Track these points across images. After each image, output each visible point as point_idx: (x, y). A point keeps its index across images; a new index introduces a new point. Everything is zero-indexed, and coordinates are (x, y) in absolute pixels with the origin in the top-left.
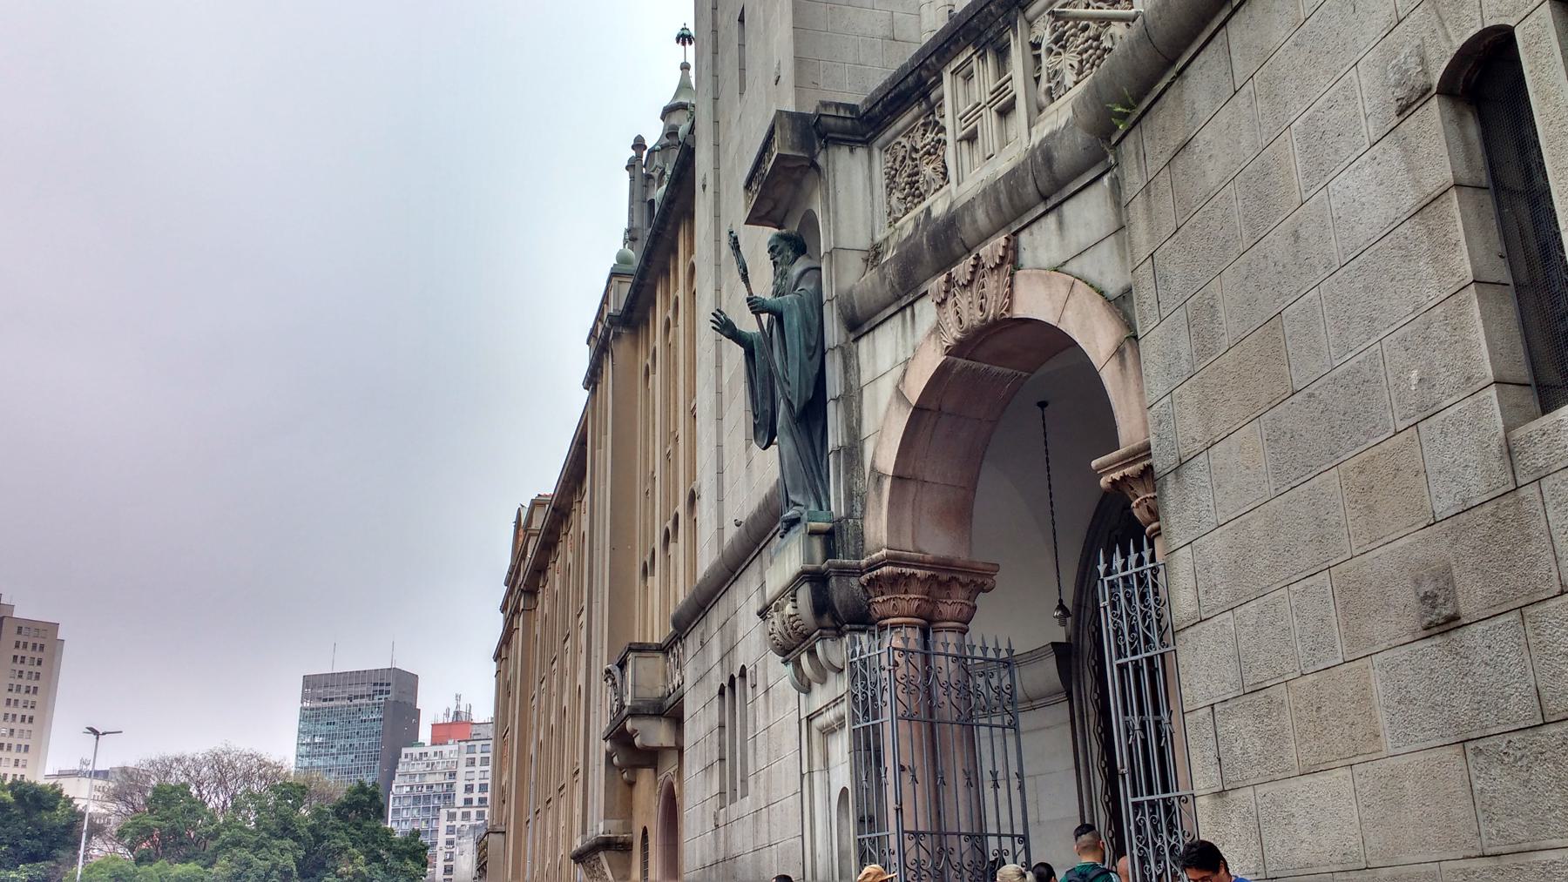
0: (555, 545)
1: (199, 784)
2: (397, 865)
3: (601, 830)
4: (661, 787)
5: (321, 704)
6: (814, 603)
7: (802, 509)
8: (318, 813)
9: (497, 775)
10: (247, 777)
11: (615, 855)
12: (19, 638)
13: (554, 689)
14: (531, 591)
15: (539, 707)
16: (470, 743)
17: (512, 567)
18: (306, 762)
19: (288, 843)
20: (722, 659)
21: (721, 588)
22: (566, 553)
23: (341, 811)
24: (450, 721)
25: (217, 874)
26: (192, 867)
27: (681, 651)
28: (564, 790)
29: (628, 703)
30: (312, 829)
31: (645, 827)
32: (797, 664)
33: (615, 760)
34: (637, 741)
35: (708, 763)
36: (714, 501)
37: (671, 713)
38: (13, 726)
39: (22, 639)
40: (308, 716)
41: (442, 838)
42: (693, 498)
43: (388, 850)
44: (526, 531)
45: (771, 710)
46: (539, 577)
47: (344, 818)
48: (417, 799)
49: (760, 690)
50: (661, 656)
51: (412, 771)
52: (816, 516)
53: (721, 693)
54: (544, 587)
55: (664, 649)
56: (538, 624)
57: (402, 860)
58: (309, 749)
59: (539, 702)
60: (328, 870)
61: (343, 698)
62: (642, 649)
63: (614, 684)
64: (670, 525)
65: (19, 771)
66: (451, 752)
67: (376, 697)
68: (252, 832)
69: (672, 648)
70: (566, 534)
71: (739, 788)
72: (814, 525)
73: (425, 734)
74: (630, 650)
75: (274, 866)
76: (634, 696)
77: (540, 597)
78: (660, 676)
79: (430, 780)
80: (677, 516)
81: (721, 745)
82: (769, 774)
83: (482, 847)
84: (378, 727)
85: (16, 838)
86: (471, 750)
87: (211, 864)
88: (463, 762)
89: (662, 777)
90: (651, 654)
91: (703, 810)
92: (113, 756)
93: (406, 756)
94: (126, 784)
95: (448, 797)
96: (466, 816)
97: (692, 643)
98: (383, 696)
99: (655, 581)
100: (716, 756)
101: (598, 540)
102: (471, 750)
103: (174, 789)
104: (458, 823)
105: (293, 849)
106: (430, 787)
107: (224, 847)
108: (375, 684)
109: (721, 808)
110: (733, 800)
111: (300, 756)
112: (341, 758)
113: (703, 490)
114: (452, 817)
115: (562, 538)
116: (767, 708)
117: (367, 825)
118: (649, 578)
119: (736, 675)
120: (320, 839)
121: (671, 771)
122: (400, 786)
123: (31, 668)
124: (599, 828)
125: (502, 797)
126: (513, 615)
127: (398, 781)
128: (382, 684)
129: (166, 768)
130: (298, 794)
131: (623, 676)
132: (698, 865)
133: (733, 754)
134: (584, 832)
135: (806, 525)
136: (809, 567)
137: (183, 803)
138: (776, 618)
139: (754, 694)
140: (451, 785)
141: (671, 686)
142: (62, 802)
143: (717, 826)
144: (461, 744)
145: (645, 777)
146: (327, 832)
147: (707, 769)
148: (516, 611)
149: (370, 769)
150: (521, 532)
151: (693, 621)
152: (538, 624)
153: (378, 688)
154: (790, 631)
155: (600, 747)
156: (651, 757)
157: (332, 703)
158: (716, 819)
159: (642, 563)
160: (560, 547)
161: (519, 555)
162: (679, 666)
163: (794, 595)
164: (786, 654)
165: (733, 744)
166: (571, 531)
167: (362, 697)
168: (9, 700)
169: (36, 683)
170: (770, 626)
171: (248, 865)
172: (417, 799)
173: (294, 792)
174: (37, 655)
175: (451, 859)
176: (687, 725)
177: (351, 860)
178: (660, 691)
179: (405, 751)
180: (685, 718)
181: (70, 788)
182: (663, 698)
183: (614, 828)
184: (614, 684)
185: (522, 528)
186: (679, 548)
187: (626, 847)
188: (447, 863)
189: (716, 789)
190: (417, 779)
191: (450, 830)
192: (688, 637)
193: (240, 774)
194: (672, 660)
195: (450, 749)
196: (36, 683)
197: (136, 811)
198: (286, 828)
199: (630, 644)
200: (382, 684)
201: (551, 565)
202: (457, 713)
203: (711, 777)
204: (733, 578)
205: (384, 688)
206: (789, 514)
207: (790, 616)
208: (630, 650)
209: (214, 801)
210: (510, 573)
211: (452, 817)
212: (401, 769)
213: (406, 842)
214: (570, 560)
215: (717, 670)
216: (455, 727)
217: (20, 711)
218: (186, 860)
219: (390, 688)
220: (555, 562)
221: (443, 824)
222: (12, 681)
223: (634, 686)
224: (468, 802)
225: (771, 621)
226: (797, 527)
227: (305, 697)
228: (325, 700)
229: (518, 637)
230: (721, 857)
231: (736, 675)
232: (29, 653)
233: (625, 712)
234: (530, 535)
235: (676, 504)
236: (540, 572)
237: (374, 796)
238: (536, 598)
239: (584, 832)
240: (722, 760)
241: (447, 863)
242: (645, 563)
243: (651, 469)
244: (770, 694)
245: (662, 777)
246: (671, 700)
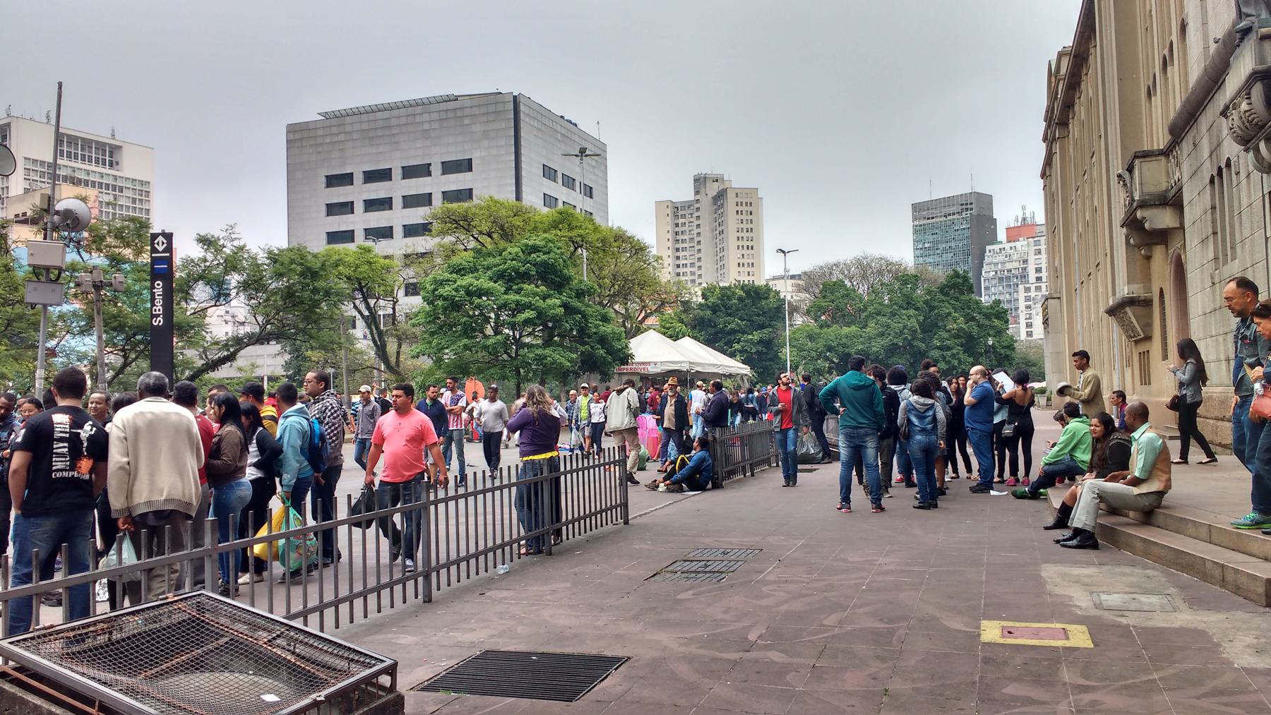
0: (1079, 84)
1: (851, 279)
2: (987, 322)
3: (1126, 292)
4: (1172, 258)
5: (926, 222)
6: (1266, 97)
7: (1253, 19)
8: (929, 292)
9: (1051, 258)
10: (880, 272)
11: (1138, 310)
12: (737, 200)
13: (1087, 194)
14: (1064, 123)
15: (1077, 210)
16: (1036, 239)
17: (1048, 107)
18: (921, 260)
19: (912, 312)
20: (1211, 155)
21: (1206, 98)
22: (1088, 87)
23: (944, 290)
24: (1019, 224)
25: (869, 332)
26: (853, 328)
27: (1179, 152)
28: (1100, 267)
29: (1137, 198)
30: (926, 302)
31: (1161, 289)
32: (1257, 151)
33: (1132, 241)
34: (1147, 226)
35: (1204, 237)
36: (1199, 25)
37: (1174, 201)
38: (743, 252)
39: (739, 200)
40: (917, 231)
41: (1022, 304)
42: (1183, 27)
43: (979, 313)
44: (1056, 77)
45: (1252, 191)
46: (1069, 112)
47: (946, 294)
48: (1001, 279)
49: (1243, 175)
50: (1163, 159)
51: (995, 261)
52: (1267, 22)
53: (1212, 181)
54: (1073, 118)
55: (1166, 153)
56: (1071, 147)
57: (990, 320)
58: (922, 251)
59: (1077, 205)
60: (940, 328)
61: (941, 216)
62: (1146, 155)
63: (1125, 185)
64: (1166, 52)
65: (751, 278)
66: (1022, 246)
67: (964, 213)
68: (887, 306)
69: (1172, 151)
70: (1087, 74)
71: (1229, 253)
72: (1263, 30)
73: (1002, 235)
74: (1136, 157)
75: (905, 327)
76: (1142, 191)
77: (1071, 126)
78: (1163, 174)
79: (1009, 266)
80: (1171, 43)
81: (1214, 222)
82: (1252, 241)
83: (1045, 309)
84: (967, 233)
85: (751, 316)
86: (1037, 243)
87: (865, 326)
88: (1032, 252)
89: (1172, 250)
90: (1154, 158)
91: (1202, 271)
92: (798, 265)
93: (990, 251)
94: (807, 280)
95: (1024, 277)
96: (1038, 289)
97: (1186, 146)
98: (969, 212)
99: (1157, 100)
100: (1210, 231)
101: (1108, 73)
102: (1037, 243)
103: (835, 283)
104: (1033, 294)
105: (916, 316)
106: (1010, 271)
107: (870, 316)
108: (962, 205)
109: (1216, 270)
110: (1225, 263)
111: (916, 257)
112: (944, 255)
113: (1190, 18)
114: (1028, 290)
115: (1084, 78)
116: (1249, 191)
117: (963, 297)
118: (1153, 98)
119: (1223, 166)
120: (932, 308)
121: (1179, 245)
122: (988, 272)
123: (747, 217)
124: (1124, 291)
125: (1055, 273)
126: (1052, 143)
127: (985, 268)
128: (967, 204)
129: (831, 268)
130: (913, 280)
131: (1132, 178)
132: (1200, 313)
133: (1223, 228)
134: (1114, 294)
135: (1257, 32)
136: (1260, 67)
137: (842, 292)
138: (1235, 115)
139: (1238, 179)
140: (1025, 269)
141: (1173, 181)
142: (772, 294)
143: (1213, 283)
144: (1030, 240)
145: (1158, 252)
146: (936, 304)
147: (1204, 241)
148: (1054, 139)
149: (965, 262)
150: (1053, 79)
151: (1186, 127)
152: (1071, 147)
153: (964, 207)
154: (1247, 124)
155: (1120, 234)
156: (1162, 237)
157: (933, 220)
158: (1212, 278)
159: (1146, 87)
160: (1083, 86)
161: (1052, 96)
162: (1178, 164)
163: (1249, 94)
164: (1248, 143)
165: (1223, 220)
166: (1090, 72)
167: (954, 214)
168: (738, 237)
169: (751, 226)
170: (1230, 122)
171: (888, 326)
172: (1001, 279)
173: (906, 279)
174: (749, 209)
175: (1030, 318)
176: (1186, 210)
177: (955, 320)
178: (1164, 186)
179: (988, 248)
180: (1185, 205)
181: (779, 286)
182: (1167, 191)
183: (1137, 290)
184: (1125, 185)
185: (1053, 75)
186: (1173, 71)
187: (1147, 303)
188: (1028, 321)
189: (1211, 255)
190: (1000, 266)
191: (1028, 299)
192: (1183, 142)
193: (875, 271)
194: (1173, 161)
195: (1021, 244)
196: (751, 226)
197: (816, 297)
198: (909, 303)
199: (1136, 153)
200: (967, 204)
201: (1077, 101)
202: (1024, 219)
203: (1208, 246)
204: (1217, 87)
205: (969, 206)
206: (1241, 25)
207: (1246, 112)
208: (1136, 157)
209: (862, 290)
210: (1047, 112)
211: (1028, 290)
212: (987, 260)
213: (992, 307)
214: (1091, 94)
215: (1208, 164)
216: (1021, 230)
217: (745, 243)
218: (848, 324)
219: (973, 206)
220: (1080, 98)
221: (1021, 295)
222: (738, 226)
223: (1141, 184)
224: (1039, 279)
225: (1231, 118)
226: (1250, 36)
227: (914, 219)
228: (928, 219)
229: (1057, 159)
230: (1218, 306)
231: (1223, 166)
232: (744, 208)
233: (1135, 204)
234: (1059, 80)
235: (1171, 34)
236: (1069, 107)
237: (966, 279)
238: (1068, 128)
239: (1114, 294)
240: (1215, 233)
241: (1028, 321)
242: (1149, 87)
243: (1148, 8)
244: (1252, 178)
245: (1172, 250)
246: (1173, 192)
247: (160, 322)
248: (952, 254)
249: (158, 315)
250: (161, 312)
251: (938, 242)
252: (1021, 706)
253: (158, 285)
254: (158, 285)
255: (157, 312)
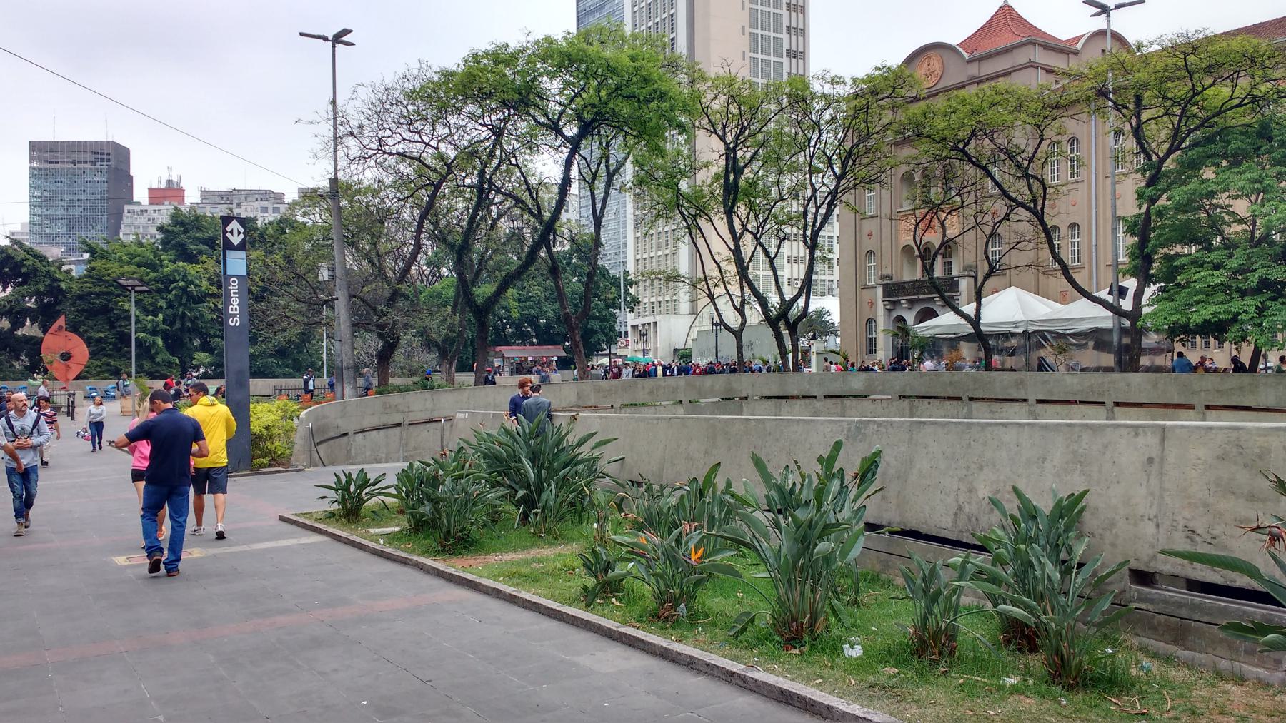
5: (48, 166)
51: (136, 223)
61: (68, 162)
128: (102, 154)
167: (85, 162)
205: (105, 157)
212: (125, 221)
219: (110, 157)
227: (32, 159)
228: (51, 163)
247: (236, 321)
248: (81, 209)
249: (235, 315)
250: (238, 312)
251: (62, 192)
252: (780, 675)
253: (234, 282)
254: (234, 282)
255: (234, 312)
